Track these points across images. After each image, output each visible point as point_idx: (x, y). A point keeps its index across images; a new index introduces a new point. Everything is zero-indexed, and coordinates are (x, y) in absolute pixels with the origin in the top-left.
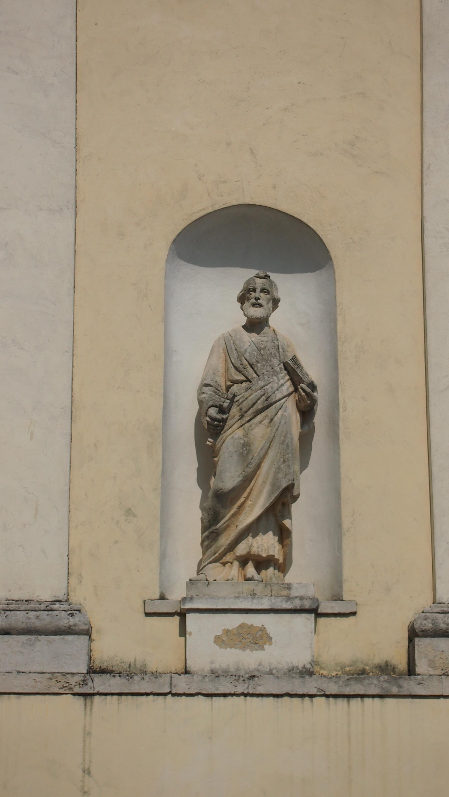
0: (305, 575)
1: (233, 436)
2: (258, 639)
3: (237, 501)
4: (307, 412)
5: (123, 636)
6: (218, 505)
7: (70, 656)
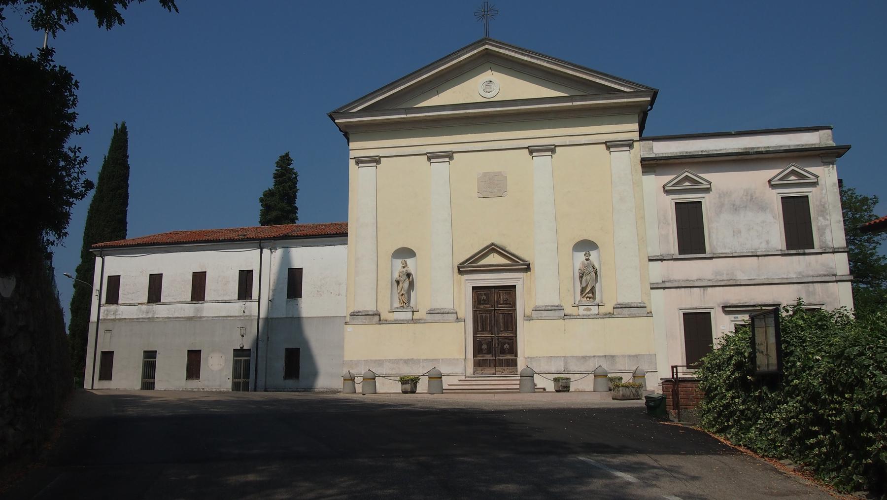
0: (597, 300)
1: (584, 278)
2: (590, 310)
3: (622, 406)
4: (596, 273)
5: (569, 310)
6: (583, 290)
7: (561, 313)
